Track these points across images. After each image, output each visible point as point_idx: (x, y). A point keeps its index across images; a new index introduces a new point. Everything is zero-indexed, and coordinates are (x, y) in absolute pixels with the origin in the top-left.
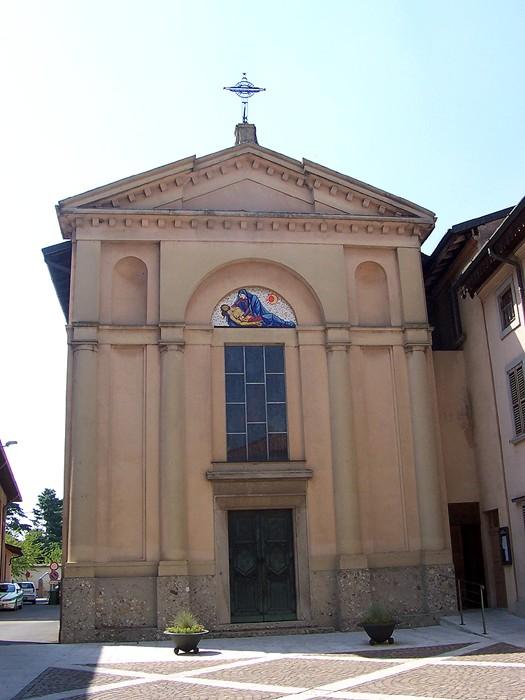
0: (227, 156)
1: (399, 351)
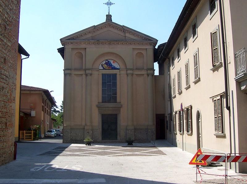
0: (103, 25)
1: (146, 76)
